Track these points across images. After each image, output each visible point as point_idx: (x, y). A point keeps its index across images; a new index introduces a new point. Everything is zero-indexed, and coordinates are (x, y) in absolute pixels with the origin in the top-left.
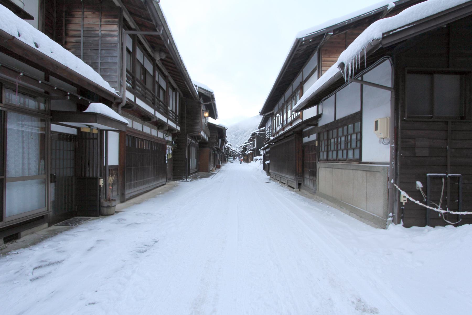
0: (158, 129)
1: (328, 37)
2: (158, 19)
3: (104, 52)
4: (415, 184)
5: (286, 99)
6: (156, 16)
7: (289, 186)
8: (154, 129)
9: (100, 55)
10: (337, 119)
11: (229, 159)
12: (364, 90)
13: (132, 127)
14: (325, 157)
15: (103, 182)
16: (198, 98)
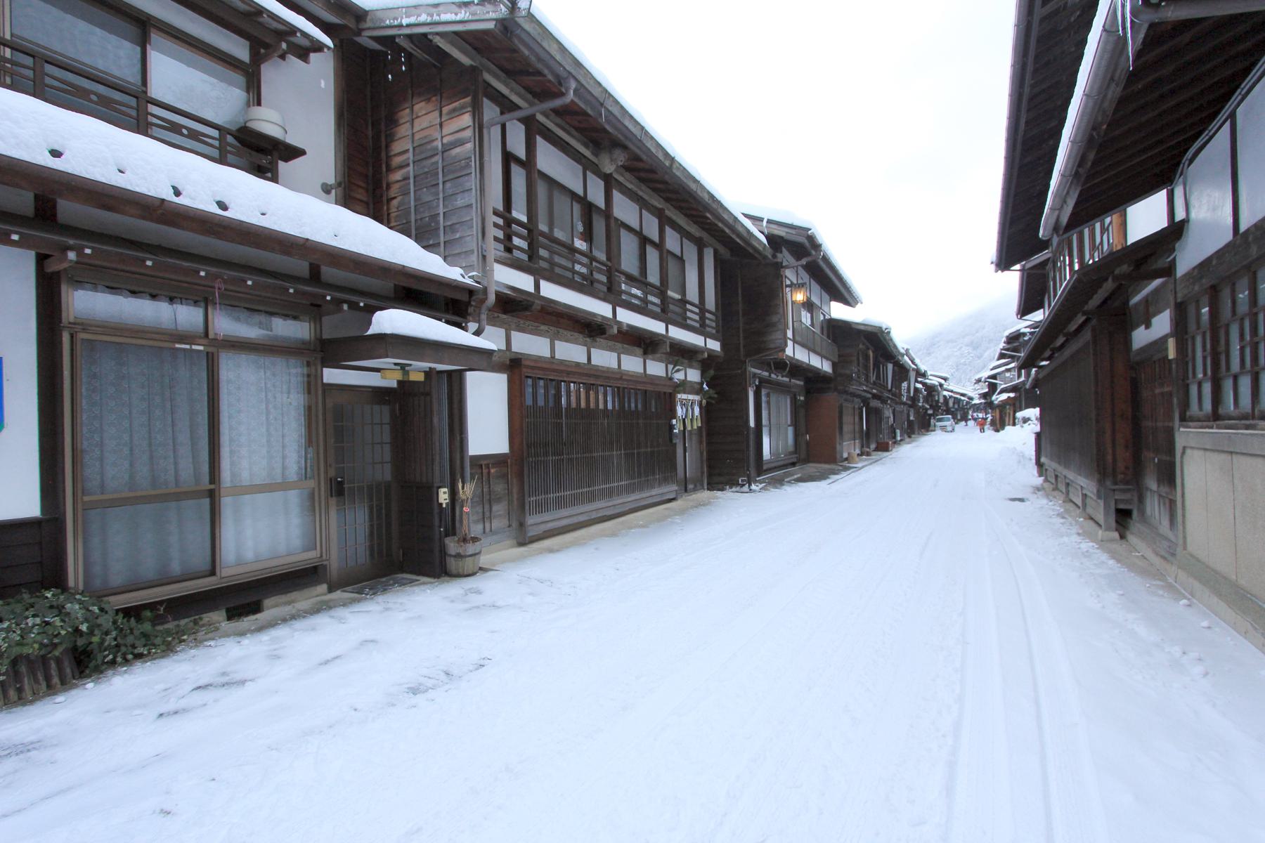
0: (645, 353)
2: (552, 63)
3: (448, 185)
6: (543, 54)
9: (441, 196)
10: (1243, 227)
11: (940, 420)
13: (553, 357)
14: (1208, 406)
15: (446, 496)
16: (769, 253)
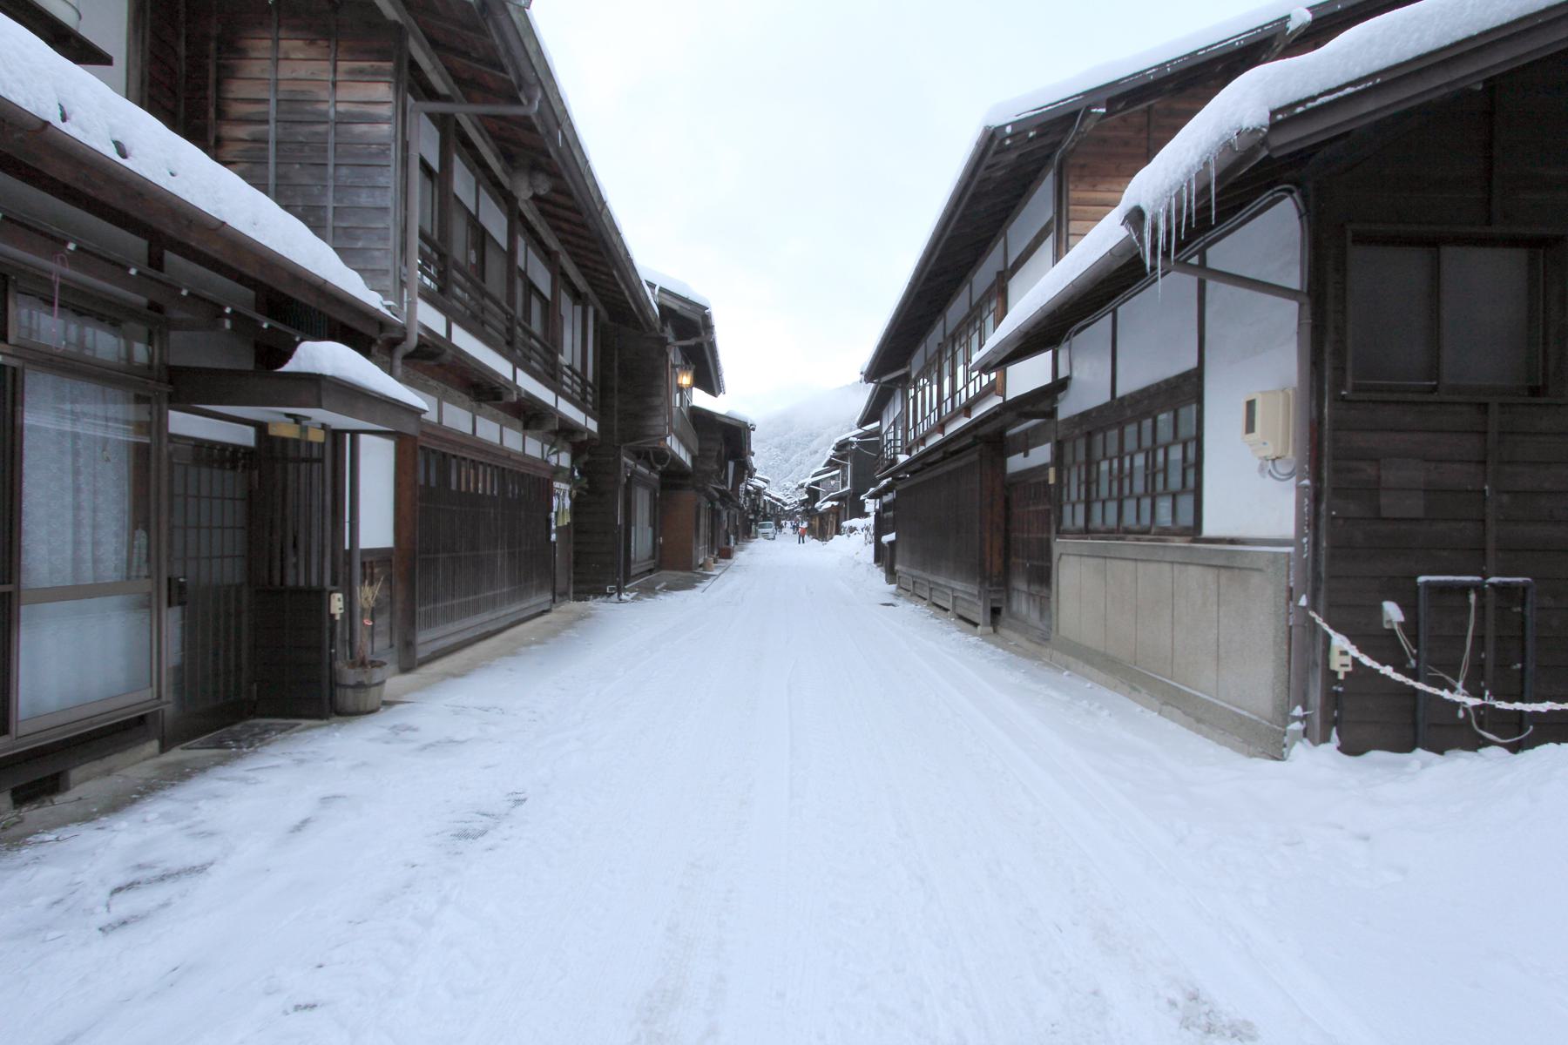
0: (526, 427)
1: (1090, 124)
2: (523, 64)
3: (344, 171)
4: (1380, 609)
5: (951, 327)
6: (518, 53)
7: (961, 617)
8: (511, 427)
9: (331, 183)
10: (1119, 394)
11: (762, 526)
12: (1208, 298)
13: (440, 422)
14: (1080, 522)
15: (341, 604)
16: (658, 325)
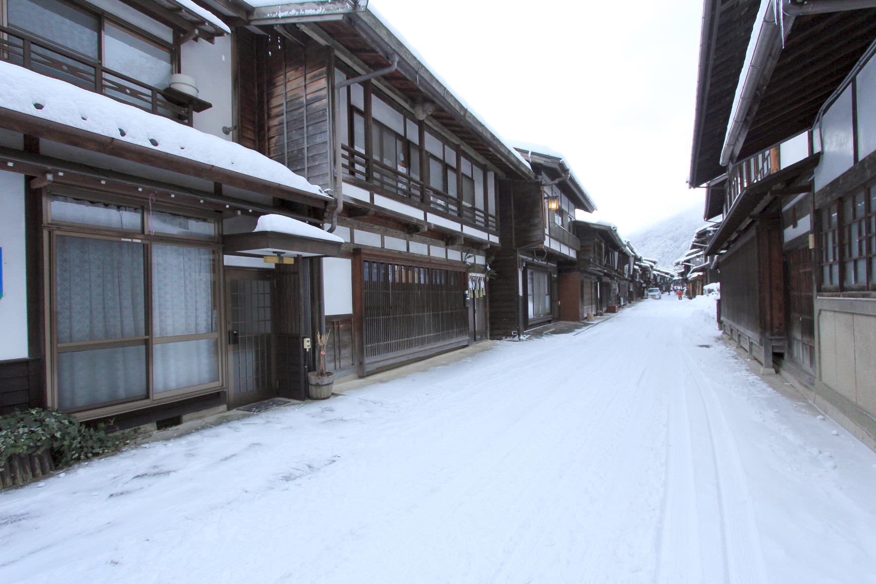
0: (447, 244)
2: (382, 43)
3: (310, 128)
6: (376, 38)
9: (305, 135)
10: (861, 157)
11: (651, 291)
13: (383, 247)
14: (836, 281)
15: (309, 344)
16: (532, 175)
